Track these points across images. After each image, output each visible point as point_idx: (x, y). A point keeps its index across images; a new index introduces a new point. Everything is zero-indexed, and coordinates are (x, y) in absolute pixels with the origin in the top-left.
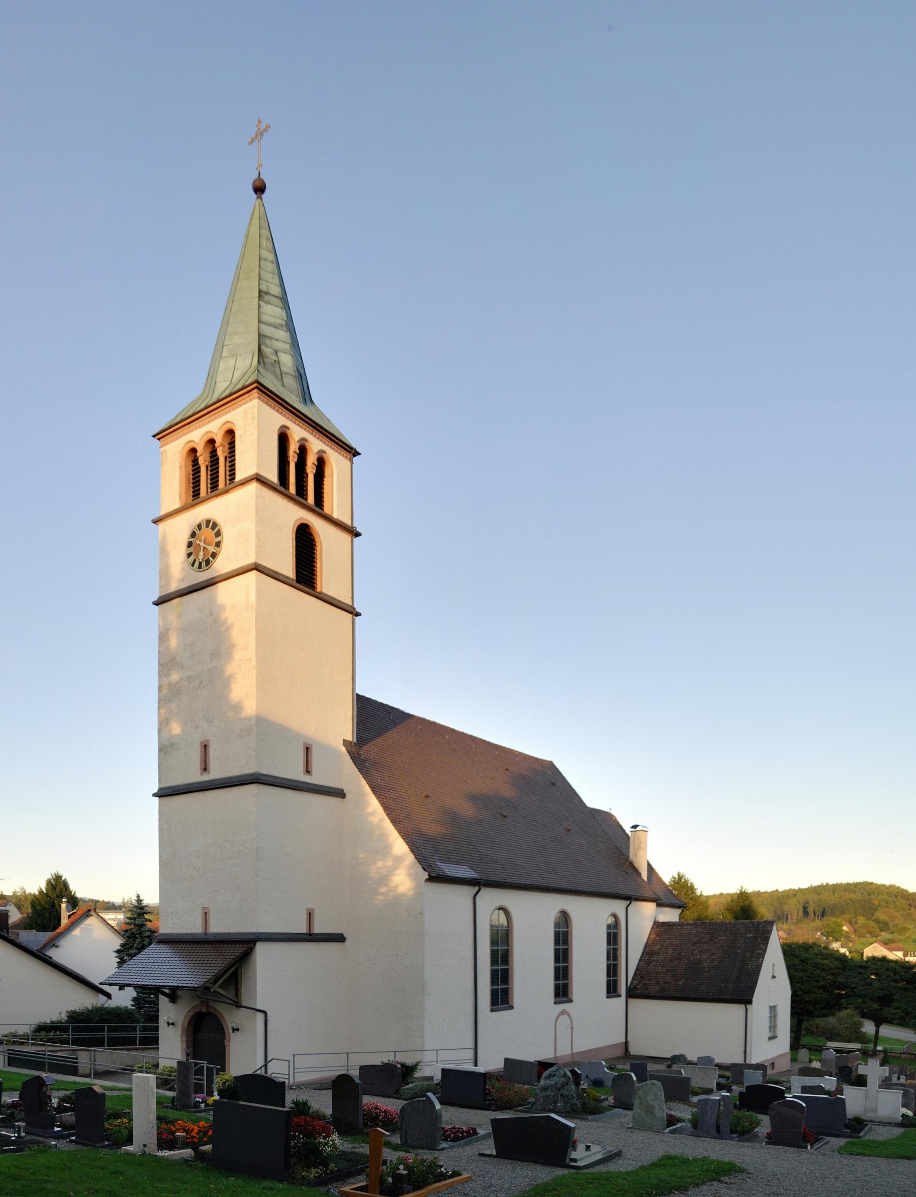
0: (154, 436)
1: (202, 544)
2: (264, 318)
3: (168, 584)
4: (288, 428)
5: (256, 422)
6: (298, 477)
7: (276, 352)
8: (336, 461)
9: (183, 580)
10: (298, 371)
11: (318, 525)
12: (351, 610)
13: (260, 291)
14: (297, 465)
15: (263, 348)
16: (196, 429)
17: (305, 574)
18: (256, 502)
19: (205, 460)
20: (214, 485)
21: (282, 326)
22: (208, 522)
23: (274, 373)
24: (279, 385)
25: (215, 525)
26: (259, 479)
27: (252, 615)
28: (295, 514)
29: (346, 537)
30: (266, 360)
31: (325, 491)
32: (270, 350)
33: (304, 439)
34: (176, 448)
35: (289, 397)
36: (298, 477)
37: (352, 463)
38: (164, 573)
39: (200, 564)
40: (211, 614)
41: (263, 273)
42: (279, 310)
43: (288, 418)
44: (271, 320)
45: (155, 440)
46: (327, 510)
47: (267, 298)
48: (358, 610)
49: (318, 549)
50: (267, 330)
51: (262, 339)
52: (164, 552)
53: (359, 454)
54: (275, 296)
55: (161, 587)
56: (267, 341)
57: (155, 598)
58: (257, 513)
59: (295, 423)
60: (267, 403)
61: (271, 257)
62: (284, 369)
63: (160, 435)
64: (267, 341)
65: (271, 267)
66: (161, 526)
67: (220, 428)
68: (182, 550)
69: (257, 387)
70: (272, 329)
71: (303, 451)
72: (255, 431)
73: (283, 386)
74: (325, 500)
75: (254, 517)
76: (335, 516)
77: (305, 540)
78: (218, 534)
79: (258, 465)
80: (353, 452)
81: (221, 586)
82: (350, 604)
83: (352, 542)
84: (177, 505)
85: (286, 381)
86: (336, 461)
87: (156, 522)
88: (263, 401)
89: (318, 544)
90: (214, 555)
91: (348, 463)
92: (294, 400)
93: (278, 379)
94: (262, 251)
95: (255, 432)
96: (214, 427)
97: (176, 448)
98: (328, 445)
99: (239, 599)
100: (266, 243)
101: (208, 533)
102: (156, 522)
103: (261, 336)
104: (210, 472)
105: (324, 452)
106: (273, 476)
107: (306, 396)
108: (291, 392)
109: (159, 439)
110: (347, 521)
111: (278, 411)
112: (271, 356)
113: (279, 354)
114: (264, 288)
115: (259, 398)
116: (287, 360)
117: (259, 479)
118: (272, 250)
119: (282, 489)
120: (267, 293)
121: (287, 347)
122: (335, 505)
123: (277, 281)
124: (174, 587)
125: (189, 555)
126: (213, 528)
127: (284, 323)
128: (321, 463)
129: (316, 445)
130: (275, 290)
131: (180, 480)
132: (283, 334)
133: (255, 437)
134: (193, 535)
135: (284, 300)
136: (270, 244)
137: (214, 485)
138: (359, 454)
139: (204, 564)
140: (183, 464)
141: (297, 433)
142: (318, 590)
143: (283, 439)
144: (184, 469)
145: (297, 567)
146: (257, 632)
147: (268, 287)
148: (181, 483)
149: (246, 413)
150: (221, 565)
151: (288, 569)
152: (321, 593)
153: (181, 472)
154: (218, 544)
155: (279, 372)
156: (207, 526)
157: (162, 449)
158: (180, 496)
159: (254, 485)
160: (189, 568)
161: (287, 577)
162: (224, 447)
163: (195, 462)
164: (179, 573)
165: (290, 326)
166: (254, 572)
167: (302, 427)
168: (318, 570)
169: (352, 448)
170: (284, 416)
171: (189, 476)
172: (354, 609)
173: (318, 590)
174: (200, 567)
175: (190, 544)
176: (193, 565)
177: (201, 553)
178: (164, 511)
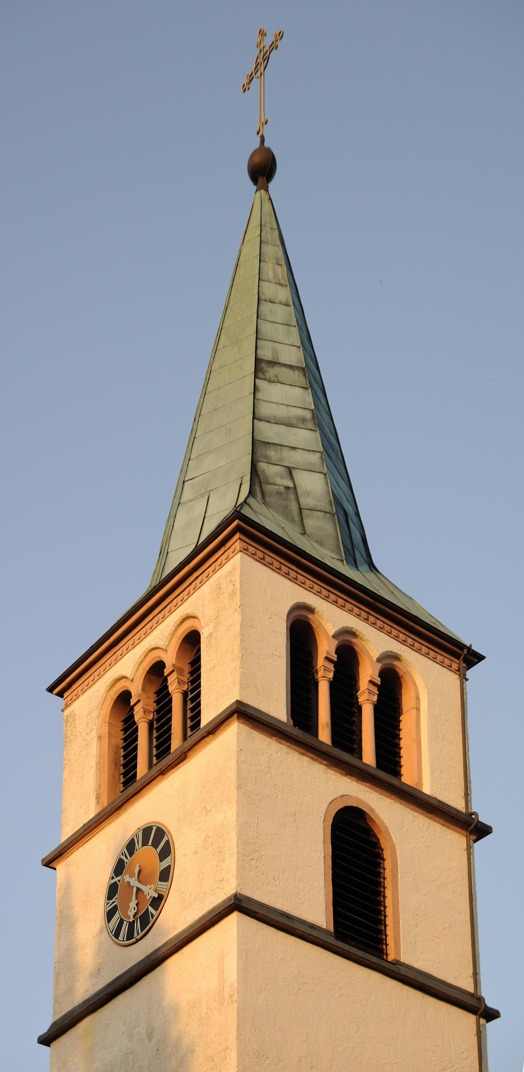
0: (50, 690)
1: (134, 882)
2: (265, 410)
3: (70, 990)
4: (311, 610)
5: (237, 600)
6: (338, 712)
7: (290, 471)
8: (426, 678)
9: (98, 971)
10: (337, 502)
11: (385, 811)
12: (473, 1002)
13: (258, 361)
14: (333, 685)
15: (262, 466)
16: (128, 650)
17: (358, 919)
18: (238, 763)
19: (145, 711)
20: (161, 747)
21: (304, 420)
22: (147, 831)
23: (285, 512)
24: (315, 552)
25: (161, 833)
26: (242, 712)
27: (230, 1016)
28: (332, 788)
29: (455, 839)
30: (268, 488)
31: (403, 743)
32: (278, 469)
33: (351, 633)
34: (92, 703)
35: (301, 531)
36: (338, 712)
37: (463, 678)
38: (65, 967)
39: (131, 925)
40: (150, 1036)
41: (265, 327)
42: (298, 391)
43: (310, 589)
44: (281, 412)
45: (53, 697)
46: (408, 777)
47: (272, 372)
48: (490, 1003)
49: (388, 864)
50: (269, 432)
51: (261, 451)
52: (66, 922)
53: (480, 658)
54: (291, 367)
55: (56, 1000)
56: (272, 453)
57: (44, 1028)
58: (239, 788)
59: (326, 598)
60: (261, 561)
61: (284, 294)
62: (306, 501)
63: (63, 686)
64: (272, 453)
65: (284, 313)
66: (61, 866)
67: (173, 635)
68: (99, 906)
69: (238, 529)
70: (282, 429)
71: (347, 657)
72: (240, 624)
73: (304, 533)
74: (403, 762)
75: (234, 794)
76: (427, 789)
77: (355, 852)
78: (166, 852)
79: (243, 687)
80: (466, 658)
81: (173, 965)
82: (471, 989)
83: (469, 849)
84: (91, 812)
85: (310, 523)
86: (426, 678)
87: (50, 863)
88: (253, 555)
89: (387, 854)
90: (158, 901)
91: (454, 679)
92: (330, 557)
93: (292, 521)
94: (264, 285)
95: (237, 619)
96: (160, 637)
97: (92, 703)
98: (404, 642)
99: (207, 981)
100: (274, 271)
101: (147, 855)
102: (50, 863)
103: (257, 446)
104: (155, 731)
105: (397, 657)
106: (278, 707)
107: (356, 546)
108: (321, 544)
109: (61, 694)
110: (458, 804)
111: (286, 575)
112: (278, 481)
113: (297, 474)
114: (266, 354)
115: (244, 550)
116: (313, 486)
117: (242, 712)
118: (285, 281)
119: (297, 732)
120: (273, 363)
121: (315, 459)
122: (428, 762)
123: (295, 338)
124: (84, 989)
125: (110, 915)
126: (155, 845)
127: (308, 415)
128: (391, 683)
129: (376, 642)
130: (293, 355)
131: (99, 763)
132: (307, 437)
133: (237, 628)
134: (119, 868)
135: (311, 374)
136: (282, 271)
137: (161, 747)
138: (480, 658)
139: (138, 925)
140: (106, 730)
141: (332, 618)
142: (390, 958)
143: (301, 633)
144: (106, 740)
145: (336, 904)
146: (241, 1054)
147: (275, 351)
148: (99, 770)
149: (219, 587)
150: (175, 917)
151: (316, 908)
152: (397, 963)
153: (100, 747)
154: (165, 875)
155: (294, 507)
156: (145, 843)
157: (67, 712)
158: (98, 797)
159: (235, 729)
160: (107, 938)
161: (313, 926)
162: (180, 671)
163: (129, 726)
164: (93, 954)
165: (322, 419)
166: (235, 917)
167: (342, 607)
168: (389, 912)
169: (461, 646)
170: (302, 585)
171: (116, 753)
172: (480, 999)
173: (390, 958)
174: (130, 935)
175: (113, 890)
176: (117, 935)
177: (133, 904)
178: (67, 832)
